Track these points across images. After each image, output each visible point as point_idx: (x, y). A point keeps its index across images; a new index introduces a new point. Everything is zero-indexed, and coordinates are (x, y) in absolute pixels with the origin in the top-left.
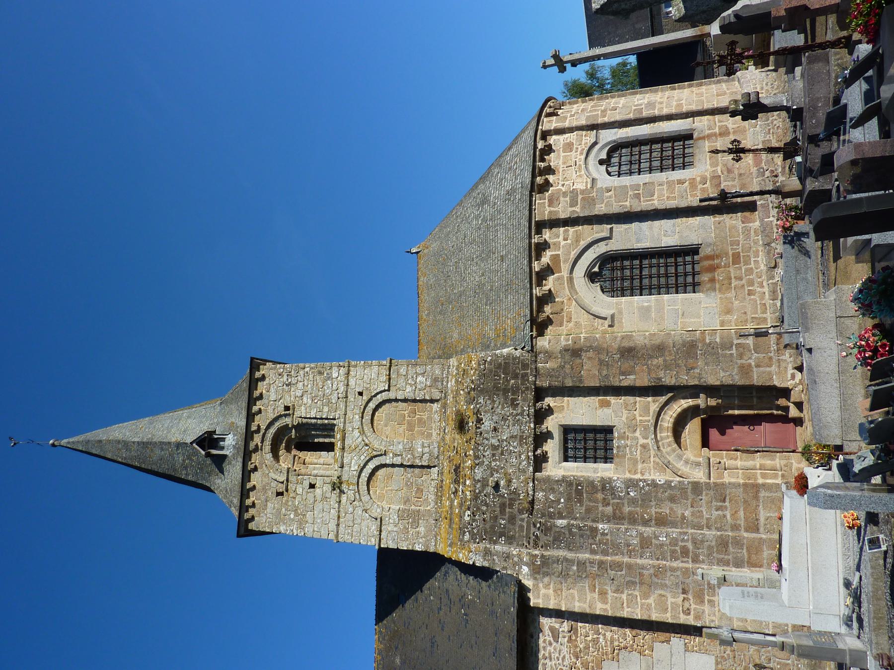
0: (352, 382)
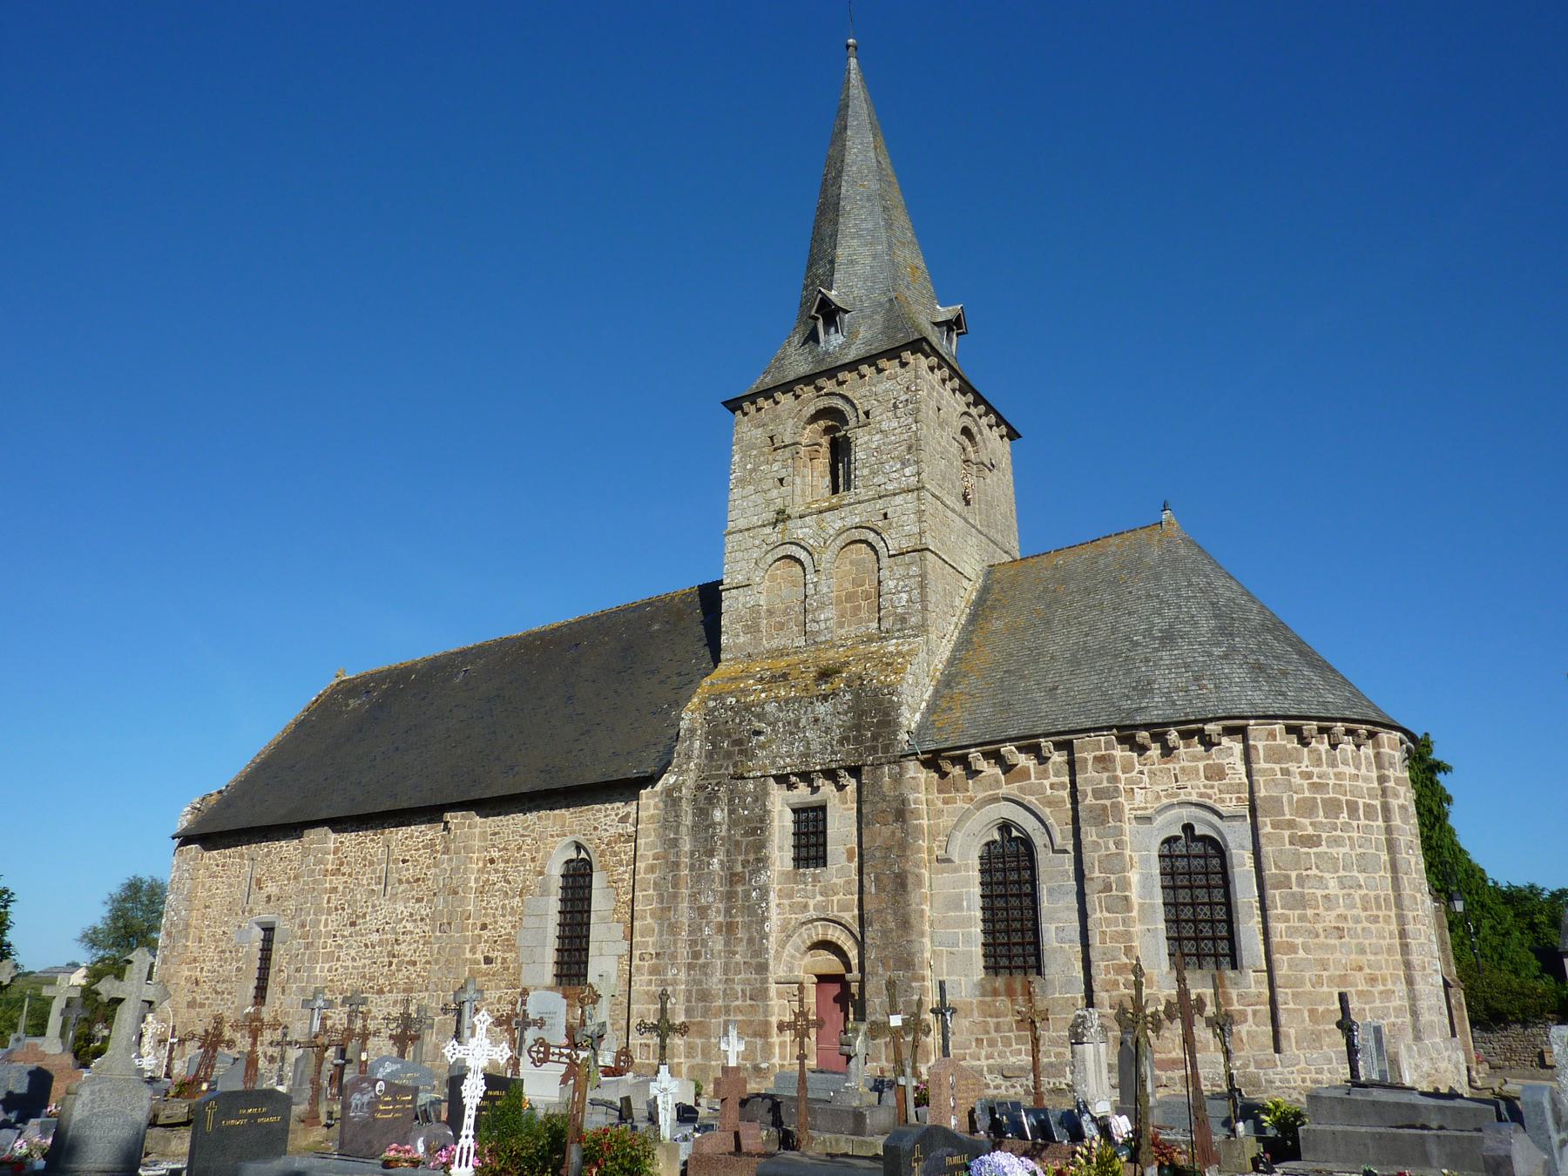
0: (899, 500)
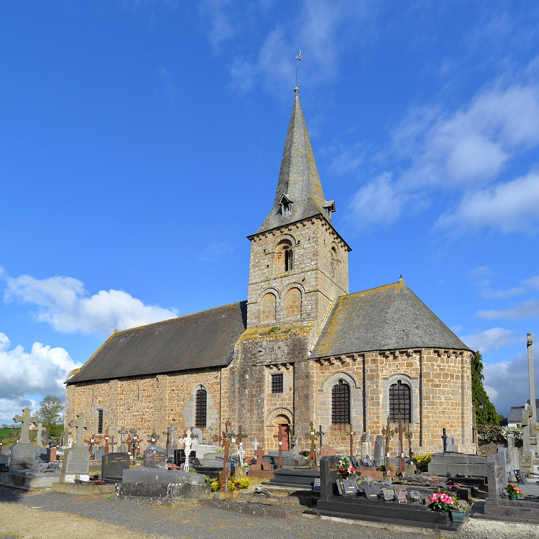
0: (309, 273)
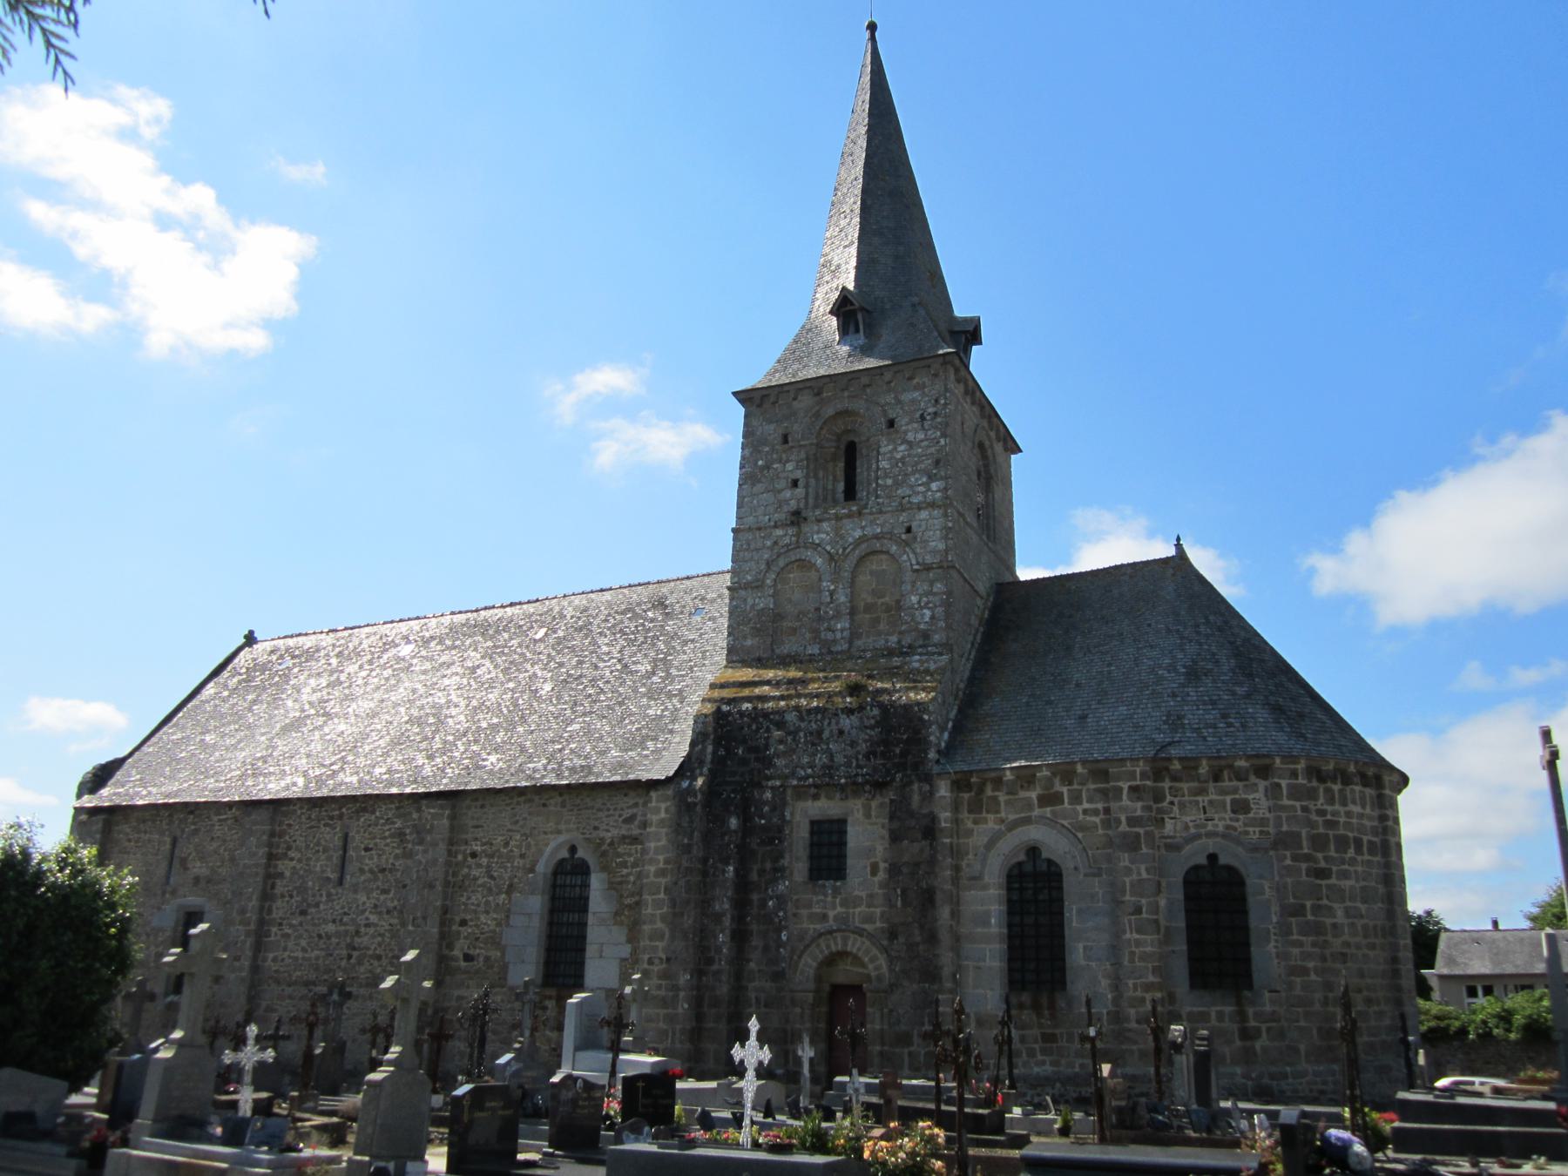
0: (924, 514)
